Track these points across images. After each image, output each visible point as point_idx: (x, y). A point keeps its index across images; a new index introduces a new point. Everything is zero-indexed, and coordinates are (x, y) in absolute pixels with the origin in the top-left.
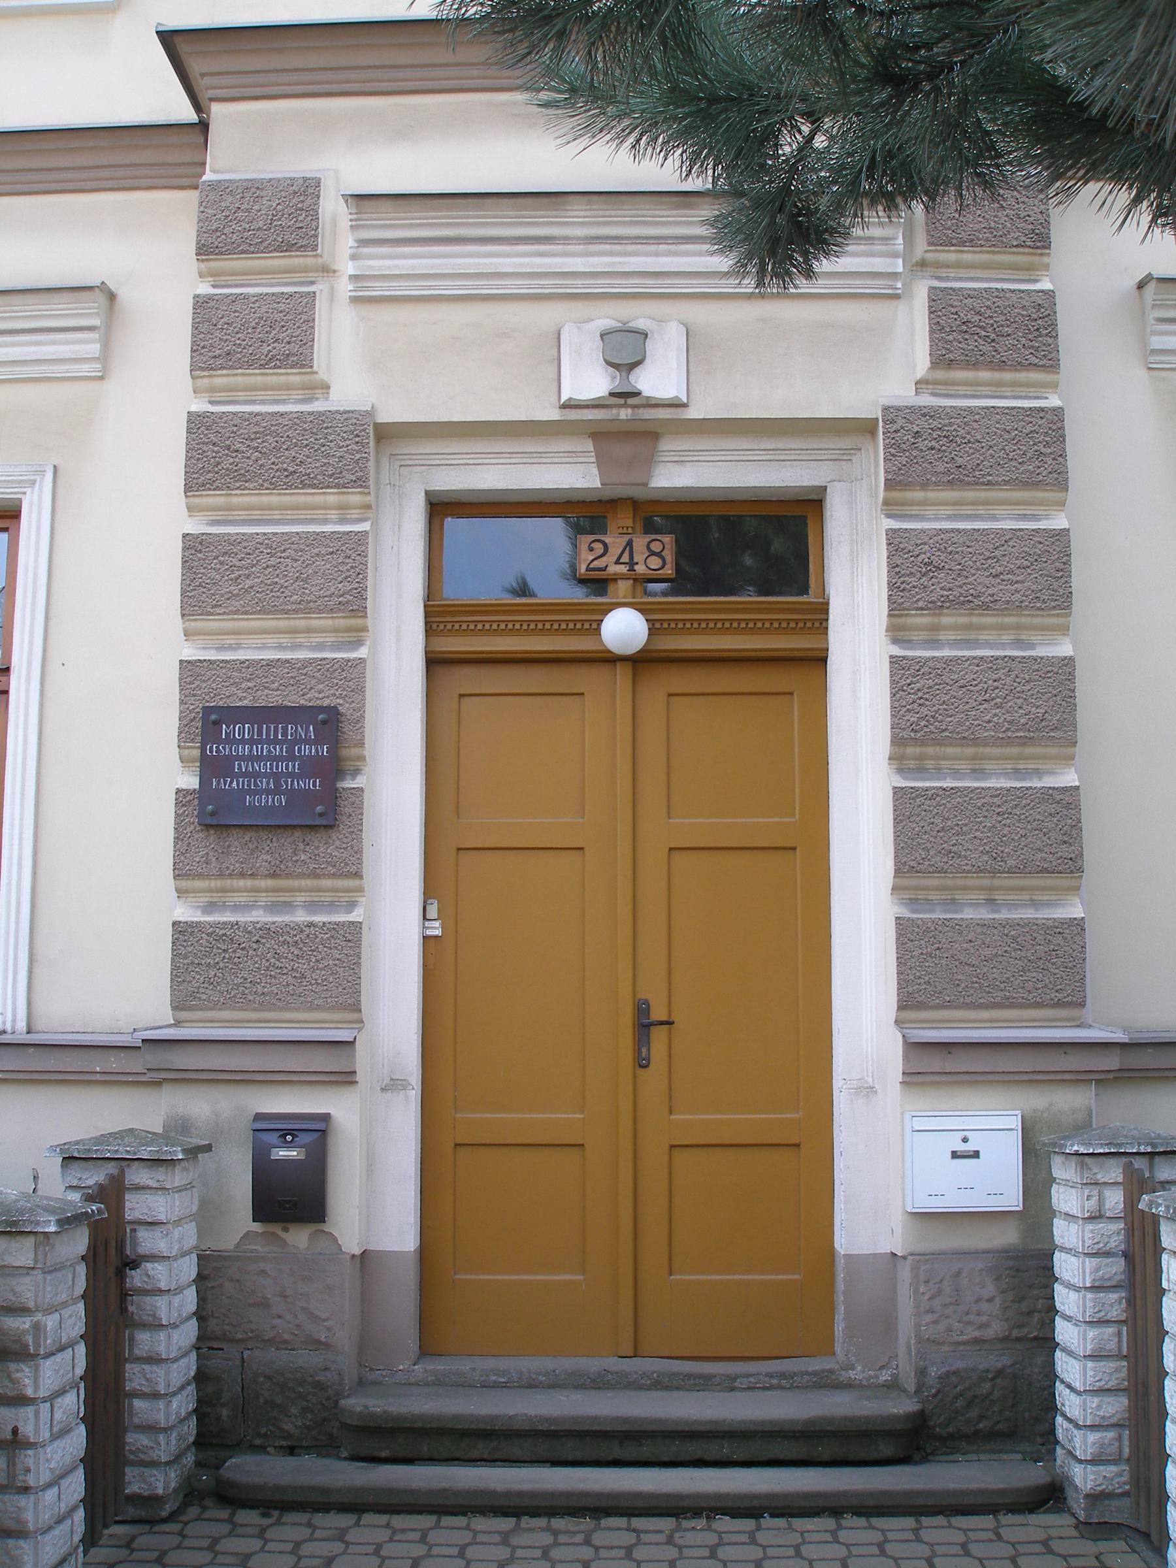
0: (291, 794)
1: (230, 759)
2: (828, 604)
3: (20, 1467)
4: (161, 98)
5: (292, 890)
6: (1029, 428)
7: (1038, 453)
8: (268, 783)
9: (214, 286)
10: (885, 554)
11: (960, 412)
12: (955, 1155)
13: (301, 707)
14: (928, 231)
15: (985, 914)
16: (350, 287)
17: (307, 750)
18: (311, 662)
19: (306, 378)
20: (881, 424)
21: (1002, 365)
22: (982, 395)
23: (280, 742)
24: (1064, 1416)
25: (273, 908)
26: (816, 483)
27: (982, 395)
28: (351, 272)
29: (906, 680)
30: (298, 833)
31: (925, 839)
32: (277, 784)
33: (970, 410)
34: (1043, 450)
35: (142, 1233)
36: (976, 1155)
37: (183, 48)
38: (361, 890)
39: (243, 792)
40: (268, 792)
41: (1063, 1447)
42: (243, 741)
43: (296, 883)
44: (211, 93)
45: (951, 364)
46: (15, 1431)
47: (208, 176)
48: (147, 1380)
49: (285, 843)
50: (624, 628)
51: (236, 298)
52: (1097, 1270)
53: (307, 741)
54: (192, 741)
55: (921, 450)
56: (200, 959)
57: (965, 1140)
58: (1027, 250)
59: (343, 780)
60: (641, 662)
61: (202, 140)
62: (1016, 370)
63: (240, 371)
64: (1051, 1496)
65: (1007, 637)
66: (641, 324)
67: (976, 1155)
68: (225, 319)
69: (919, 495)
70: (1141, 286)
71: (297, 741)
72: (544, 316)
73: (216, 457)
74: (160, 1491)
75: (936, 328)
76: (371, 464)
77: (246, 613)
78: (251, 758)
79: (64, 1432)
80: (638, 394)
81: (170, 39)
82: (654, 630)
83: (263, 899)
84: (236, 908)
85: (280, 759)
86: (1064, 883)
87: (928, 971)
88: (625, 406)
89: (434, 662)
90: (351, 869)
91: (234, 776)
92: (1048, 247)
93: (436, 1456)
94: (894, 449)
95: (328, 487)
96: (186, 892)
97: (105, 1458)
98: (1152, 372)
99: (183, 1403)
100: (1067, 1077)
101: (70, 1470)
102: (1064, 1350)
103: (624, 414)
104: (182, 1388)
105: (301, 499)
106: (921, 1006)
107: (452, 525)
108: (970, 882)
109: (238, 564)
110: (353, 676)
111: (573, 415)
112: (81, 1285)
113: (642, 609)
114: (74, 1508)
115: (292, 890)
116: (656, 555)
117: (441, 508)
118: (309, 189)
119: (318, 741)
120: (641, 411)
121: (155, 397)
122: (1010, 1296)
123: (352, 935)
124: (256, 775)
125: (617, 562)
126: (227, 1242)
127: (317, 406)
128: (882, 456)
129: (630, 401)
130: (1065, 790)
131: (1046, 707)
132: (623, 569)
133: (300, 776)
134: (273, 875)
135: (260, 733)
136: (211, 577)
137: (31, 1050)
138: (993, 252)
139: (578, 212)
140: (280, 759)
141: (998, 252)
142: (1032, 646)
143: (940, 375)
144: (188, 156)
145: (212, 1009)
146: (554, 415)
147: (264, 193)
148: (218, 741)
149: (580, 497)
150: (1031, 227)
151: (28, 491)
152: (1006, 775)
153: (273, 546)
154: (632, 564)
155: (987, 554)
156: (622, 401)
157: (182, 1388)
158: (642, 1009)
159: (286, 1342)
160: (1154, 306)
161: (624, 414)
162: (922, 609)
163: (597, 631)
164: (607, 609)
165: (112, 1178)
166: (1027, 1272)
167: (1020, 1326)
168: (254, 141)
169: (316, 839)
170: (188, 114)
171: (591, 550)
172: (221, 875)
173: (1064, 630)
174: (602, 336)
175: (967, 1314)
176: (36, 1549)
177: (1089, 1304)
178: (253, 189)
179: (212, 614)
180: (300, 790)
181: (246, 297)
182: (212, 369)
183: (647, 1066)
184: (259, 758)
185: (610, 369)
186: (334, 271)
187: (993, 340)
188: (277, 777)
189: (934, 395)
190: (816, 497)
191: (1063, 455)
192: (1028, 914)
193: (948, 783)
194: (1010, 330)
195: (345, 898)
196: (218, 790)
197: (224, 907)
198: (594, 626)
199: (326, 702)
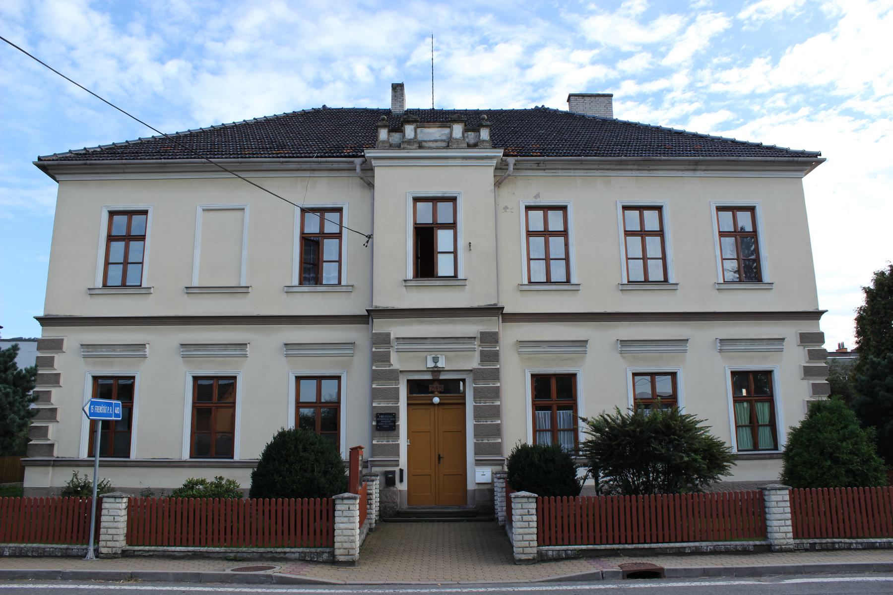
7: (495, 375)
31: (479, 431)
50: (436, 400)
55: (478, 374)
60: (439, 404)
72: (426, 353)
73: (376, 376)
87: (478, 449)
89: (408, 404)
90: (397, 436)
116: (441, 387)
118: (389, 334)
131: (496, 412)
136: (375, 394)
139: (428, 341)
166: (492, 491)
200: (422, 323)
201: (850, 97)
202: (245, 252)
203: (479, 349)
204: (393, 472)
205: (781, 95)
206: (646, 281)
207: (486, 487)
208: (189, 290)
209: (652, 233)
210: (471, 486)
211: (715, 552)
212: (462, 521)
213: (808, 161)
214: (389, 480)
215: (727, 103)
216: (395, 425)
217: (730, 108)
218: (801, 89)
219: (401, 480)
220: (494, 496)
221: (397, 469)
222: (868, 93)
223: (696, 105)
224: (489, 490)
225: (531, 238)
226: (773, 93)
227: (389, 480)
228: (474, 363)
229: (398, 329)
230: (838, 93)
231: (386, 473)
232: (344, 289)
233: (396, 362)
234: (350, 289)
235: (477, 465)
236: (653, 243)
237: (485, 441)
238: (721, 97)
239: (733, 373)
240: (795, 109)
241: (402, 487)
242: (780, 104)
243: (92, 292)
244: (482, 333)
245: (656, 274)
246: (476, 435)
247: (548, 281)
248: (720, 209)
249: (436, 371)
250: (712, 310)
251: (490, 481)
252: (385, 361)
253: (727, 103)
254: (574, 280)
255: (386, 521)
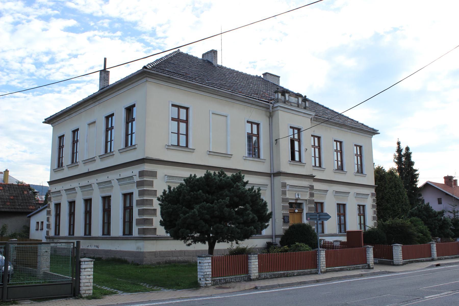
50: (297, 211)
201: (145, 33)
202: (211, 134)
205: (107, 21)
206: (178, 145)
208: (211, 153)
209: (183, 121)
211: (299, 275)
213: (373, 132)
215: (75, 16)
217: (76, 19)
218: (120, 20)
222: (153, 34)
223: (56, 12)
226: (103, 18)
229: (290, 182)
230: (139, 28)
236: (183, 126)
238: (73, 11)
239: (337, 204)
240: (114, 31)
242: (106, 25)
243: (170, 147)
245: (183, 143)
247: (178, 145)
248: (173, 105)
250: (234, 168)
253: (75, 16)
254: (190, 146)
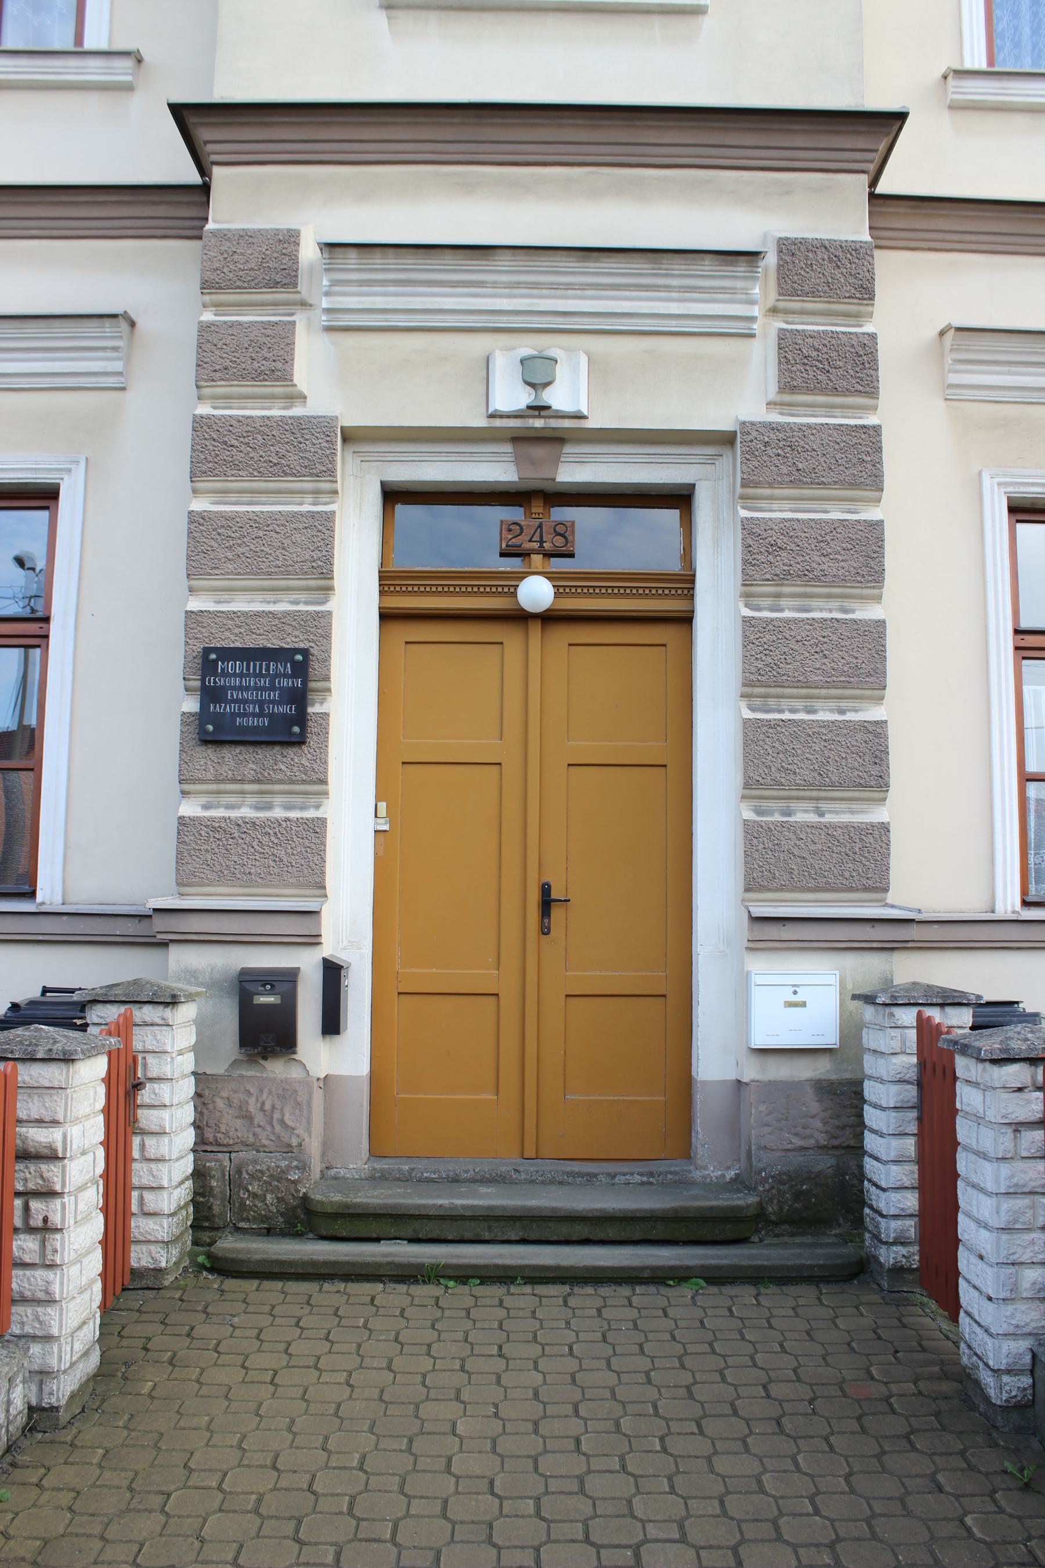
0: (271, 716)
1: (224, 689)
2: (694, 576)
3: (49, 1248)
4: (171, 163)
5: (271, 793)
6: (854, 440)
7: (860, 460)
8: (254, 708)
9: (216, 315)
10: (740, 536)
11: (801, 428)
12: (790, 1004)
13: (282, 649)
14: (779, 285)
15: (812, 818)
16: (324, 318)
17: (286, 683)
18: (287, 613)
19: (288, 389)
20: (739, 435)
21: (835, 391)
22: (815, 415)
23: (265, 676)
24: (871, 1207)
25: (257, 808)
26: (687, 482)
27: (815, 415)
28: (325, 305)
29: (754, 635)
30: (277, 748)
31: (771, 763)
32: (261, 709)
33: (809, 426)
34: (865, 458)
35: (151, 1060)
36: (803, 1004)
37: (191, 120)
38: (326, 793)
39: (234, 715)
40: (254, 715)
41: (870, 1232)
42: (235, 675)
43: (277, 787)
44: (214, 158)
45: (793, 389)
46: (46, 1220)
47: (210, 226)
48: (153, 1176)
49: (267, 756)
51: (232, 325)
52: (899, 1094)
53: (285, 676)
54: (195, 674)
55: (760, 455)
56: (198, 847)
57: (795, 993)
58: (856, 301)
59: (313, 705)
60: (549, 618)
61: (205, 199)
62: (845, 396)
63: (235, 383)
64: (859, 1270)
65: (835, 604)
66: (552, 353)
67: (803, 1004)
68: (224, 341)
69: (768, 492)
70: (942, 334)
71: (277, 675)
72: (478, 344)
73: (216, 451)
74: (163, 1265)
75: (784, 360)
76: (339, 458)
77: (239, 574)
78: (241, 688)
79: (87, 1218)
80: (549, 408)
81: (180, 112)
82: (557, 595)
83: (251, 800)
84: (228, 807)
85: (263, 689)
86: (876, 795)
87: (766, 859)
88: (539, 417)
89: (386, 617)
90: (317, 780)
91: (227, 702)
92: (872, 299)
93: (382, 1235)
94: (750, 453)
95: (304, 476)
96: (189, 793)
97: (116, 1241)
98: (949, 403)
99: (183, 1193)
100: (875, 945)
101: (88, 1252)
102: (871, 1156)
103: (539, 423)
104: (182, 1183)
105: (283, 485)
106: (762, 889)
107: (400, 509)
108: (801, 793)
109: (233, 535)
110: (320, 625)
111: (498, 423)
112: (101, 1102)
113: (550, 576)
114: (93, 1282)
115: (271, 793)
117: (394, 496)
118: (290, 239)
119: (294, 675)
120: (552, 420)
121: (161, 406)
122: (829, 1113)
123: (317, 829)
124: (245, 701)
125: (530, 541)
126: (218, 1068)
127: (297, 411)
128: (739, 460)
129: (543, 413)
130: (877, 723)
132: (536, 545)
133: (279, 703)
134: (258, 781)
135: (248, 668)
136: (209, 546)
137: (65, 918)
138: (829, 302)
139: (504, 262)
140: (263, 689)
141: (833, 302)
142: (853, 611)
143: (787, 398)
144: (194, 212)
145: (209, 885)
146: (482, 422)
147: (255, 240)
148: (215, 674)
149: (502, 489)
150: (860, 282)
151: (66, 477)
152: (831, 711)
153: (256, 521)
154: (541, 541)
155: (820, 538)
156: (537, 413)
157: (182, 1183)
158: (546, 890)
159: (265, 1146)
160: (951, 350)
161: (539, 423)
162: (768, 580)
163: (514, 595)
164: (522, 576)
165: (125, 1015)
166: (845, 1098)
167: (836, 1138)
168: (247, 199)
169: (291, 752)
170: (193, 177)
171: (510, 530)
172: (218, 781)
173: (878, 599)
174: (522, 361)
175: (795, 1127)
176: (61, 1315)
177: (892, 1121)
178: (246, 237)
179: (211, 574)
180: (279, 714)
181: (240, 324)
182: (213, 380)
183: (548, 933)
184: (247, 689)
185: (528, 388)
186: (311, 305)
187: (828, 372)
188: (261, 703)
189: (781, 414)
190: (685, 493)
191: (880, 463)
192: (845, 818)
193: (787, 716)
194: (841, 364)
195: (313, 800)
196: (215, 713)
197: (217, 806)
198: (512, 590)
199: (302, 645)
200: (468, 188)
203: (768, 330)
204: (285, 981)
207: (805, 1071)
210: (713, 1062)
212: (679, 1276)
214: (264, 1028)
216: (301, 718)
219: (332, 1023)
220: (859, 1126)
221: (307, 964)
224: (824, 1088)
225: (675, 566)
227: (264, 1028)
228: (742, 391)
231: (246, 985)
232: (93, 70)
233: (325, 379)
234: (121, 70)
235: (756, 946)
237: (804, 816)
241: (338, 1060)
244: (788, 248)
246: (758, 780)
249: (539, 433)
251: (830, 1038)
252: (260, 376)
255: (224, 1268)
